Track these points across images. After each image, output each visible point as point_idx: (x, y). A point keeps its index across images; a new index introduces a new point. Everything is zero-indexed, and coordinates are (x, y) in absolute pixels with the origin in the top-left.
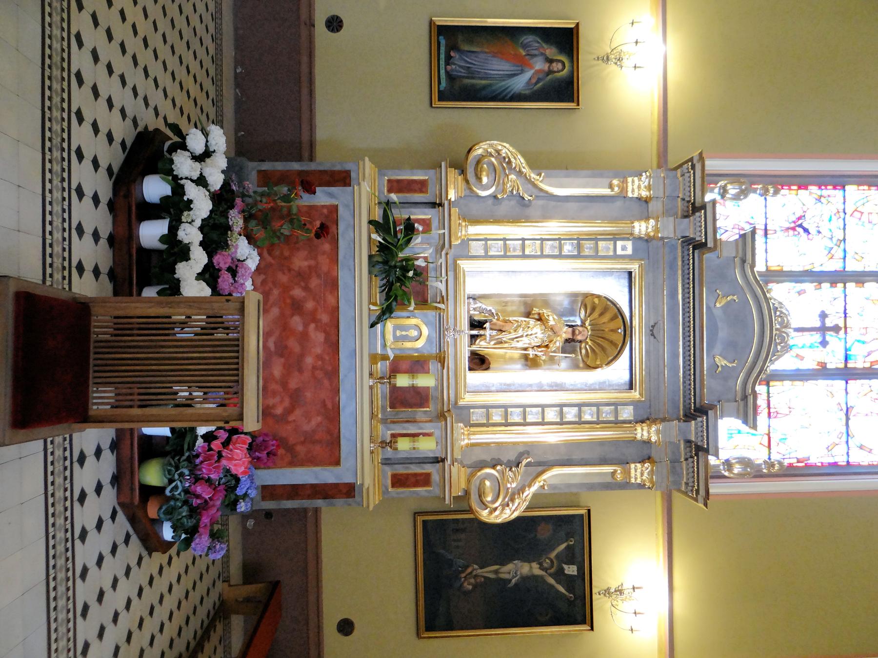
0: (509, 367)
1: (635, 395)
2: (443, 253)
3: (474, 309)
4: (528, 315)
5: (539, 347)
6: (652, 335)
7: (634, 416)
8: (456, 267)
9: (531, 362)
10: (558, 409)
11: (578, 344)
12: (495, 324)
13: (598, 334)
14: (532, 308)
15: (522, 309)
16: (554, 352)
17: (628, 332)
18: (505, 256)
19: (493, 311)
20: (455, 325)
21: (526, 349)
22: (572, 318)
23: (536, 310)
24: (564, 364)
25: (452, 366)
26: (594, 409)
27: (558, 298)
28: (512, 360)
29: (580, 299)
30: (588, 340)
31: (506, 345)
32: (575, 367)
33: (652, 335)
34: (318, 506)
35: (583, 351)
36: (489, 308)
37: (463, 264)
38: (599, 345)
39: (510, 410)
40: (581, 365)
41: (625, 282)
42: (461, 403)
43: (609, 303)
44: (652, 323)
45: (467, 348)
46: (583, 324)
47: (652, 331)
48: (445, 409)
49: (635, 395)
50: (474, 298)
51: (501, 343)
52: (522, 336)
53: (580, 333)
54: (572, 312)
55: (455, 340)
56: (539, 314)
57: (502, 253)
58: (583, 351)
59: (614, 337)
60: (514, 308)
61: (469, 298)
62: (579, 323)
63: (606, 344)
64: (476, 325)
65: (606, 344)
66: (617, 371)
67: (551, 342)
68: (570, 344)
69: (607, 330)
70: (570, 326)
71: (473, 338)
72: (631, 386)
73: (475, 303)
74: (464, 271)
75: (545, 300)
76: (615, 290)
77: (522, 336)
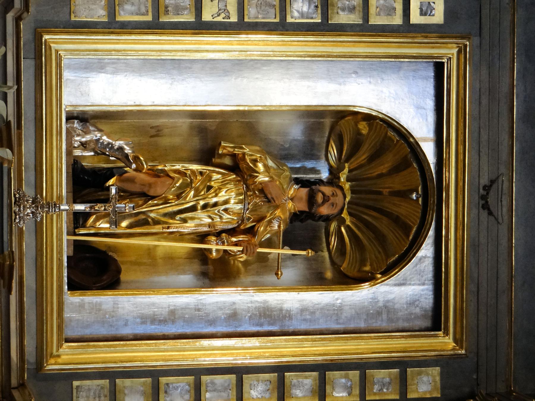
0: (163, 279)
1: (445, 343)
2: (10, 17)
3: (84, 145)
4: (207, 156)
5: (232, 232)
6: (486, 206)
7: (443, 387)
8: (38, 51)
9: (216, 272)
10: (273, 376)
11: (323, 224)
12: (131, 180)
13: (366, 200)
14: (217, 141)
15: (196, 142)
16: (269, 244)
17: (433, 200)
18: (155, 26)
19: (128, 150)
20: (38, 187)
21: (202, 237)
22: (309, 164)
23: (226, 147)
24: (289, 274)
25: (29, 280)
26: (355, 374)
27: (277, 121)
28: (171, 262)
29: (328, 122)
30: (345, 215)
31: (157, 229)
32: (316, 280)
33: (486, 206)
34: (423, 17)
35: (333, 241)
36: (117, 144)
37: (58, 42)
38: (368, 225)
39: (163, 380)
40: (329, 274)
41: (428, 87)
42: (52, 366)
43: (391, 133)
44: (485, 181)
45: (65, 237)
46: (334, 180)
47: (485, 198)
48: (14, 382)
49: (445, 343)
50: (83, 118)
51: (145, 223)
52: (193, 209)
53: (326, 199)
54: (309, 151)
55: (38, 227)
56: (234, 156)
57: (149, 18)
58: (333, 241)
59: (402, 209)
60: (177, 141)
61: (68, 119)
62: (325, 175)
63: (383, 225)
64: (87, 183)
65: (383, 225)
66: (408, 288)
67: (260, 220)
68: (303, 230)
69: (386, 191)
70: (302, 183)
71: (79, 220)
72: (436, 321)
73: (86, 132)
74: (59, 59)
75: (246, 124)
76: (404, 101)
77: (193, 209)
